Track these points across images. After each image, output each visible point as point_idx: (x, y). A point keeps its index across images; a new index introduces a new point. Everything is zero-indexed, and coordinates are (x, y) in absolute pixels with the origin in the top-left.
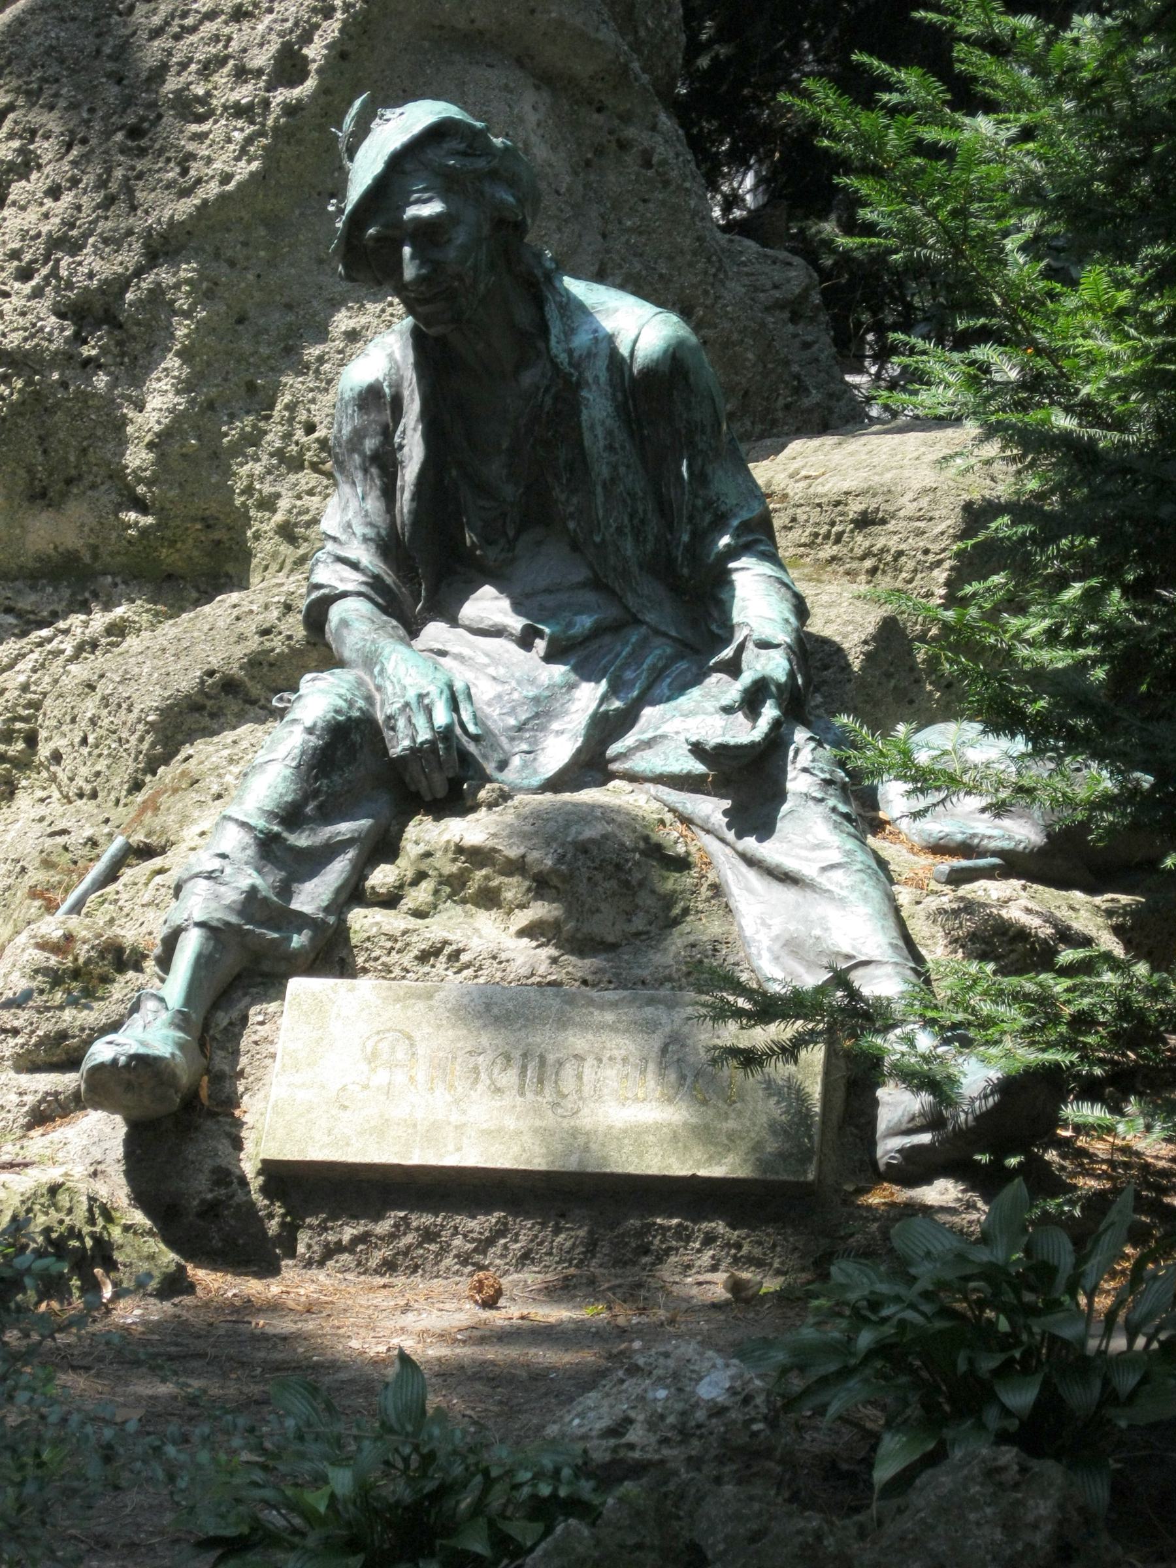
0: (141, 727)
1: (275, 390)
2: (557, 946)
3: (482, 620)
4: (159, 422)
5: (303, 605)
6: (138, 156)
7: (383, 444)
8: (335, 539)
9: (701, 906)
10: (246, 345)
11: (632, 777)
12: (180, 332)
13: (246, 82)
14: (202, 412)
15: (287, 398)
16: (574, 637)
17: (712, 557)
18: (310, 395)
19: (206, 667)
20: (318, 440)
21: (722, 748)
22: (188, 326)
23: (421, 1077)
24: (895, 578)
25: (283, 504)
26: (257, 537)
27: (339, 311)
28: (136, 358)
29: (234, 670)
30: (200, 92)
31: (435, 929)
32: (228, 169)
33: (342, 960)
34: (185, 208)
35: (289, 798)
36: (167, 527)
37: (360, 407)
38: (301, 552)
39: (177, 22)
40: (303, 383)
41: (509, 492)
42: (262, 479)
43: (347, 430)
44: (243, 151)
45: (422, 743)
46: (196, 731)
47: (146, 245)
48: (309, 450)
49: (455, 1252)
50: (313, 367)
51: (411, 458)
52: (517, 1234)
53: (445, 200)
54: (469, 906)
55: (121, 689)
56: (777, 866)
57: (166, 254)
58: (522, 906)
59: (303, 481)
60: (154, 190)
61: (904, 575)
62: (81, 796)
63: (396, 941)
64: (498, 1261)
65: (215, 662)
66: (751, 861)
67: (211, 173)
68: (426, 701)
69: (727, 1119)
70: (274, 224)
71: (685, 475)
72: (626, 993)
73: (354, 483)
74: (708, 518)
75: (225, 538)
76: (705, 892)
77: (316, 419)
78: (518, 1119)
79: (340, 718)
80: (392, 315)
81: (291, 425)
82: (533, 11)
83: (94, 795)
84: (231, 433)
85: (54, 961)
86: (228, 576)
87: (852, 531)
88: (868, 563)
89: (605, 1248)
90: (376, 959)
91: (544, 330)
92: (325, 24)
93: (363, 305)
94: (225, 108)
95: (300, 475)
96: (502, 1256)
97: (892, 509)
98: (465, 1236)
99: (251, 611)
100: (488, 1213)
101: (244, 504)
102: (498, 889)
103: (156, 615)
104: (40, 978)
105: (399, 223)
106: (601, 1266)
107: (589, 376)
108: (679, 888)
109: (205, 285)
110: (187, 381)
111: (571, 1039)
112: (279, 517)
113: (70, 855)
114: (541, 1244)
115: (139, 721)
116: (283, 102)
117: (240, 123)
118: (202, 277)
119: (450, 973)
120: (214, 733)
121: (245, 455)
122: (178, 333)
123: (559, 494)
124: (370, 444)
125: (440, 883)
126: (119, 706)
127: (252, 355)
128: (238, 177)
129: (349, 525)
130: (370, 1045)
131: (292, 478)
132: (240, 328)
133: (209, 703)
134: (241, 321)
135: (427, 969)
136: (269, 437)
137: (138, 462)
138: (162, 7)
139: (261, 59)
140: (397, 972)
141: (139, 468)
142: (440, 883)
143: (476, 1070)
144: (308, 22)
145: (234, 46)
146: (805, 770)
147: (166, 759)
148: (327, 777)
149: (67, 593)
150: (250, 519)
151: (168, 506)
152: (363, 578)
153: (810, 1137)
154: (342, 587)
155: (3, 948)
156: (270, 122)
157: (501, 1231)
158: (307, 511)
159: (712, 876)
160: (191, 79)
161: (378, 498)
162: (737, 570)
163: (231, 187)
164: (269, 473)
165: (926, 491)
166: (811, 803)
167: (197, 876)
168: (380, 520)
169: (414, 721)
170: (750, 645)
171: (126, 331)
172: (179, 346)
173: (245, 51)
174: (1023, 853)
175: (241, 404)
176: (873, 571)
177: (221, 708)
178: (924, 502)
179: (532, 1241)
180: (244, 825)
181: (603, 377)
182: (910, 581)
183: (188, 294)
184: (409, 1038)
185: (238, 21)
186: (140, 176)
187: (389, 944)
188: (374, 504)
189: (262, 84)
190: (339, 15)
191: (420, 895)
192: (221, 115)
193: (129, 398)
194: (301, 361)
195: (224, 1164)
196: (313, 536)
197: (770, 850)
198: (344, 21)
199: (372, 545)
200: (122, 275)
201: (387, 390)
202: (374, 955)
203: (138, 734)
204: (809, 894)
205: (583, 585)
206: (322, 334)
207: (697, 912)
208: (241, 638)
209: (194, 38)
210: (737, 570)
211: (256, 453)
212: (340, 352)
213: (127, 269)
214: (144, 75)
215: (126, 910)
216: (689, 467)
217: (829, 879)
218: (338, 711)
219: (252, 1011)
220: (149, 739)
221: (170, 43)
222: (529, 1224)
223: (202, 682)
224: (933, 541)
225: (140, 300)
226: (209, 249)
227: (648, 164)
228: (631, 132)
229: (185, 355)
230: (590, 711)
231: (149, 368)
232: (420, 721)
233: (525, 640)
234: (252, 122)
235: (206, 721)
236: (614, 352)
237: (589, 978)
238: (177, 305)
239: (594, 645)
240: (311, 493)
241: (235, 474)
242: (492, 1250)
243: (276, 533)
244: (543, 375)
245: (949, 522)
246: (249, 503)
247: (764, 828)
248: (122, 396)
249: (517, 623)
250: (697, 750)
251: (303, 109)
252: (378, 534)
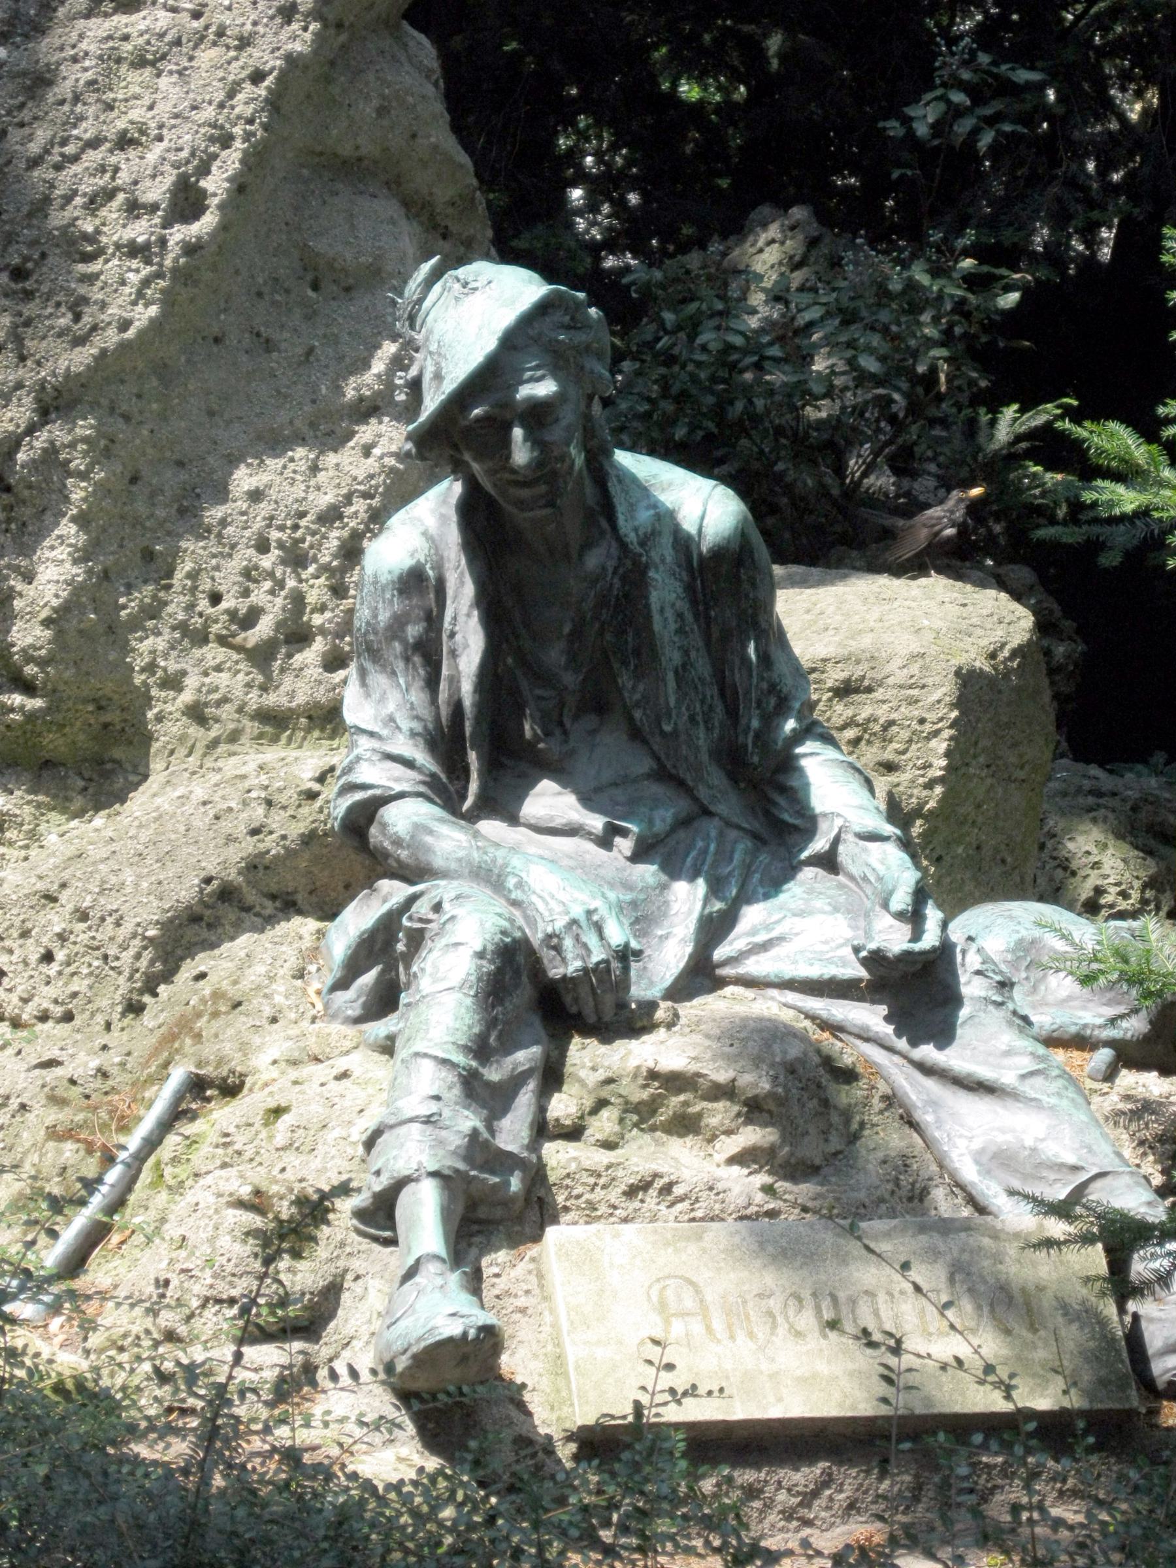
0: (137, 942)
1: (175, 554)
2: (770, 1173)
3: (552, 818)
4: (57, 596)
6: (22, 300)
7: (428, 630)
8: (372, 734)
9: (875, 1119)
10: (141, 508)
11: (749, 982)
12: (76, 496)
13: (138, 217)
14: (98, 585)
15: (188, 566)
16: (656, 835)
17: (780, 743)
18: (214, 562)
19: (203, 874)
20: (227, 611)
22: (86, 489)
23: (718, 1325)
24: (884, 748)
25: (192, 681)
26: (159, 718)
27: (237, 467)
28: (24, 524)
29: (233, 875)
30: (90, 229)
32: (125, 315)
33: (540, 1200)
34: (80, 359)
35: (476, 1030)
36: (58, 710)
37: (401, 592)
38: (213, 734)
39: (56, 150)
40: (204, 548)
42: (166, 656)
43: (384, 617)
44: (140, 294)
45: (598, 964)
46: (196, 944)
47: (38, 400)
48: (216, 621)
49: (780, 1508)
50: (216, 530)
51: (466, 646)
52: (842, 1484)
53: (556, 378)
54: (658, 1133)
55: (102, 901)
56: (969, 1075)
57: (57, 408)
58: (729, 1132)
59: (209, 656)
60: (44, 338)
61: (895, 745)
62: (44, 1017)
63: (599, 1176)
64: (823, 1514)
65: (211, 867)
66: (927, 1069)
67: (107, 319)
68: (595, 918)
69: (1035, 1348)
70: (163, 371)
71: (753, 657)
72: (895, 1222)
73: (394, 673)
74: (773, 701)
75: (117, 720)
76: (877, 1104)
77: (222, 588)
78: (829, 1362)
79: (508, 940)
80: (295, 472)
81: (193, 595)
82: (414, 136)
83: (68, 1017)
84: (130, 605)
85: (257, 1221)
86: (117, 762)
87: (830, 700)
88: (850, 733)
89: (929, 1492)
90: (578, 1197)
92: (224, 154)
93: (262, 461)
94: (118, 246)
95: (205, 649)
96: (828, 1508)
97: (880, 677)
98: (789, 1490)
99: (230, 809)
100: (812, 1462)
101: (144, 683)
102: (699, 1115)
103: (39, 806)
104: (251, 1241)
105: (507, 404)
106: (928, 1510)
107: (655, 555)
108: (853, 1101)
109: (103, 443)
110: (84, 549)
111: (856, 1274)
112: (187, 697)
113: (80, 1089)
114: (866, 1492)
115: (134, 935)
116: (183, 241)
117: (135, 263)
118: (100, 434)
119: (662, 1207)
120: (213, 946)
121: (145, 629)
122: (74, 497)
123: (625, 679)
124: (413, 631)
125: (625, 1111)
126: (103, 919)
127: (148, 518)
128: (137, 324)
129: (391, 719)
130: (654, 1293)
131: (197, 653)
132: (134, 488)
133: (208, 912)
134: (134, 480)
135: (637, 1204)
136: (170, 609)
137: (29, 640)
138: (39, 133)
139: (156, 191)
140: (603, 1209)
141: (32, 646)
142: (625, 1111)
143: (770, 1314)
144: (205, 152)
145: (123, 178)
146: (978, 973)
147: (167, 976)
148: (502, 1004)
150: (151, 698)
151: (61, 687)
152: (421, 778)
153: (1122, 1362)
154: (398, 788)
156: (168, 263)
157: (826, 1482)
158: (216, 689)
159: (883, 1088)
160: (76, 214)
161: (422, 689)
162: (805, 755)
163: (131, 333)
164: (173, 648)
165: (914, 657)
166: (991, 1008)
167: (411, 1120)
168: (425, 712)
169: (584, 939)
170: (849, 837)
171: (16, 495)
172: (75, 511)
173: (136, 183)
174: (1130, 1041)
175: (136, 573)
176: (856, 742)
177: (217, 918)
178: (915, 669)
179: (857, 1490)
180: (444, 1062)
182: (904, 752)
183: (85, 454)
184: (691, 1283)
185: (122, 149)
186: (28, 323)
187: (592, 1180)
188: (418, 696)
189: (157, 221)
190: (238, 144)
191: (604, 1124)
192: (113, 255)
193: (17, 569)
194: (200, 525)
195: (524, 1432)
196: (224, 716)
197: (951, 1058)
198: (245, 151)
199: (420, 741)
200: (13, 432)
201: (431, 573)
202: (575, 1192)
203: (132, 952)
204: (1010, 1102)
205: (648, 776)
206: (222, 494)
207: (873, 1125)
208: (230, 839)
209: (76, 168)
210: (805, 755)
211: (156, 627)
212: (243, 514)
213: (18, 426)
214: (25, 209)
215: (248, 1155)
216: (756, 649)
217: (1032, 1087)
218: (504, 933)
219: (484, 1262)
220: (148, 955)
221: (51, 175)
222: (853, 1472)
223: (201, 891)
224: (929, 710)
225: (34, 461)
226: (104, 402)
229: (82, 520)
230: (695, 915)
231: (41, 534)
232: (592, 940)
233: (605, 841)
234: (148, 262)
235: (205, 934)
236: (677, 530)
237: (810, 1204)
238: (72, 465)
239: (672, 842)
240: (218, 669)
241: (133, 650)
242: (817, 1503)
243: (183, 714)
244: (608, 556)
245: (944, 690)
246: (151, 681)
247: (944, 1035)
248: (9, 566)
249: (596, 822)
251: (201, 247)
252: (425, 727)
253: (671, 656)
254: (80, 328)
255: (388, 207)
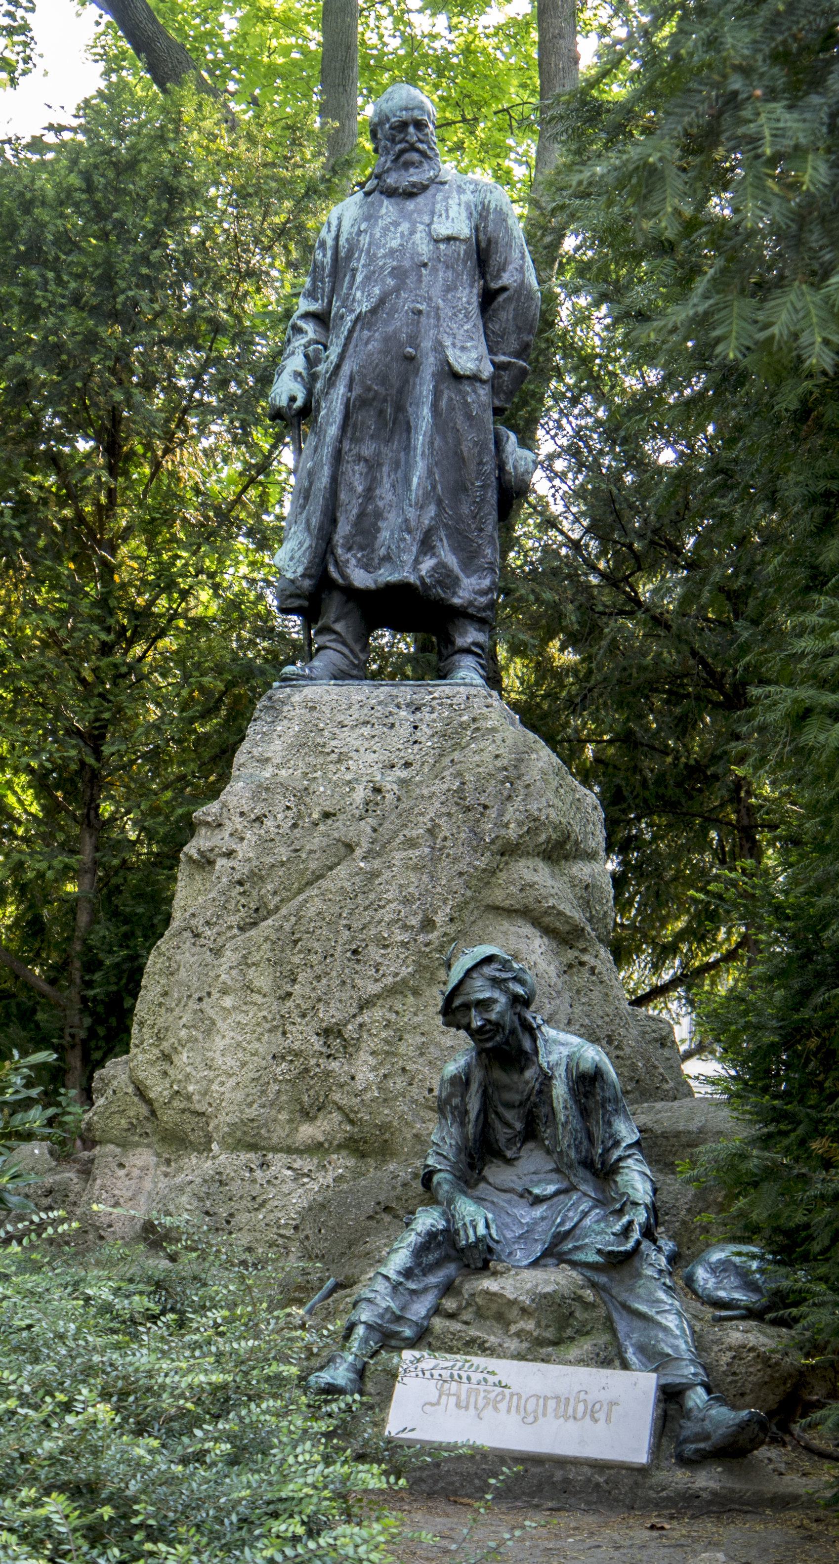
5: (422, 1173)
21: (611, 1253)
31: (473, 1332)
41: (518, 1126)
74: (611, 1143)
91: (536, 1052)
149: (315, 1161)
155: (833, 1241)
181: (563, 1074)
227: (593, 974)
228: (585, 958)
239: (555, 1199)
250: (599, 1252)
253: (561, 1117)
254: (378, 976)
255: (527, 929)
